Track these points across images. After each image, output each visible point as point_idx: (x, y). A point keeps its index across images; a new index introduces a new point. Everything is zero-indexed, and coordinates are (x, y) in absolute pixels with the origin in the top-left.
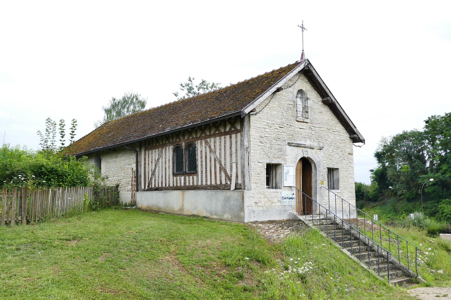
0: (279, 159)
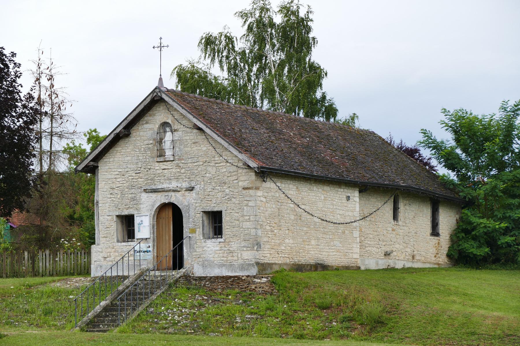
0: (131, 210)
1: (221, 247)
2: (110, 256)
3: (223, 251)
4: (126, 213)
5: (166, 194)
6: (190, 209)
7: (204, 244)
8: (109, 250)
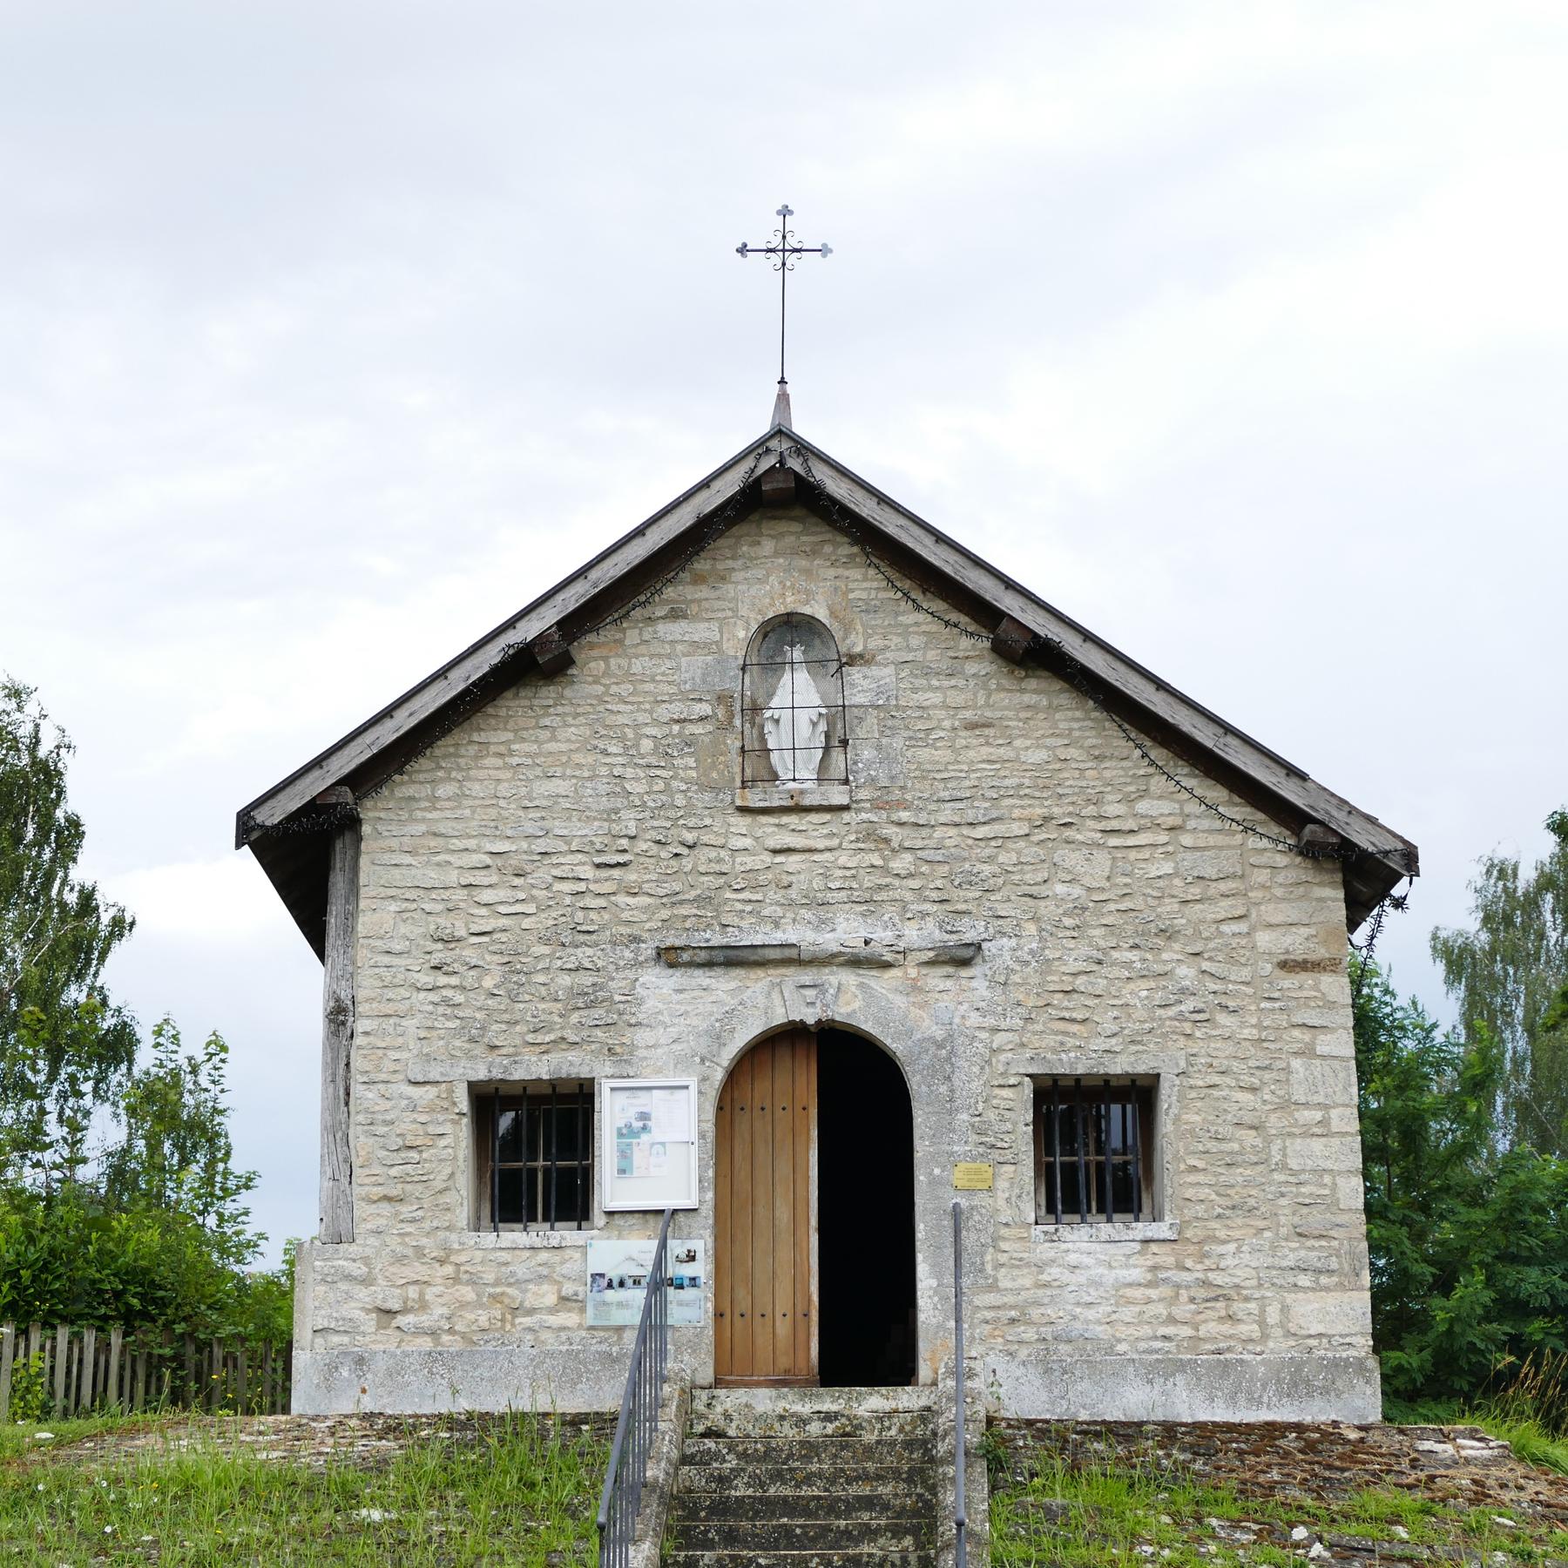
0: (572, 1055)
8: (418, 1270)
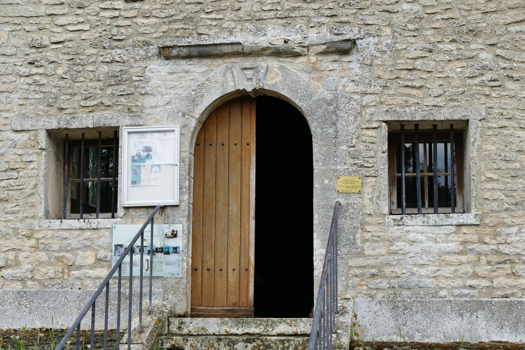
0: (107, 113)
1: (464, 243)
2: (17, 263)
3: (472, 257)
4: (86, 121)
5: (247, 65)
6: (342, 114)
7: (395, 231)
8: (14, 242)
